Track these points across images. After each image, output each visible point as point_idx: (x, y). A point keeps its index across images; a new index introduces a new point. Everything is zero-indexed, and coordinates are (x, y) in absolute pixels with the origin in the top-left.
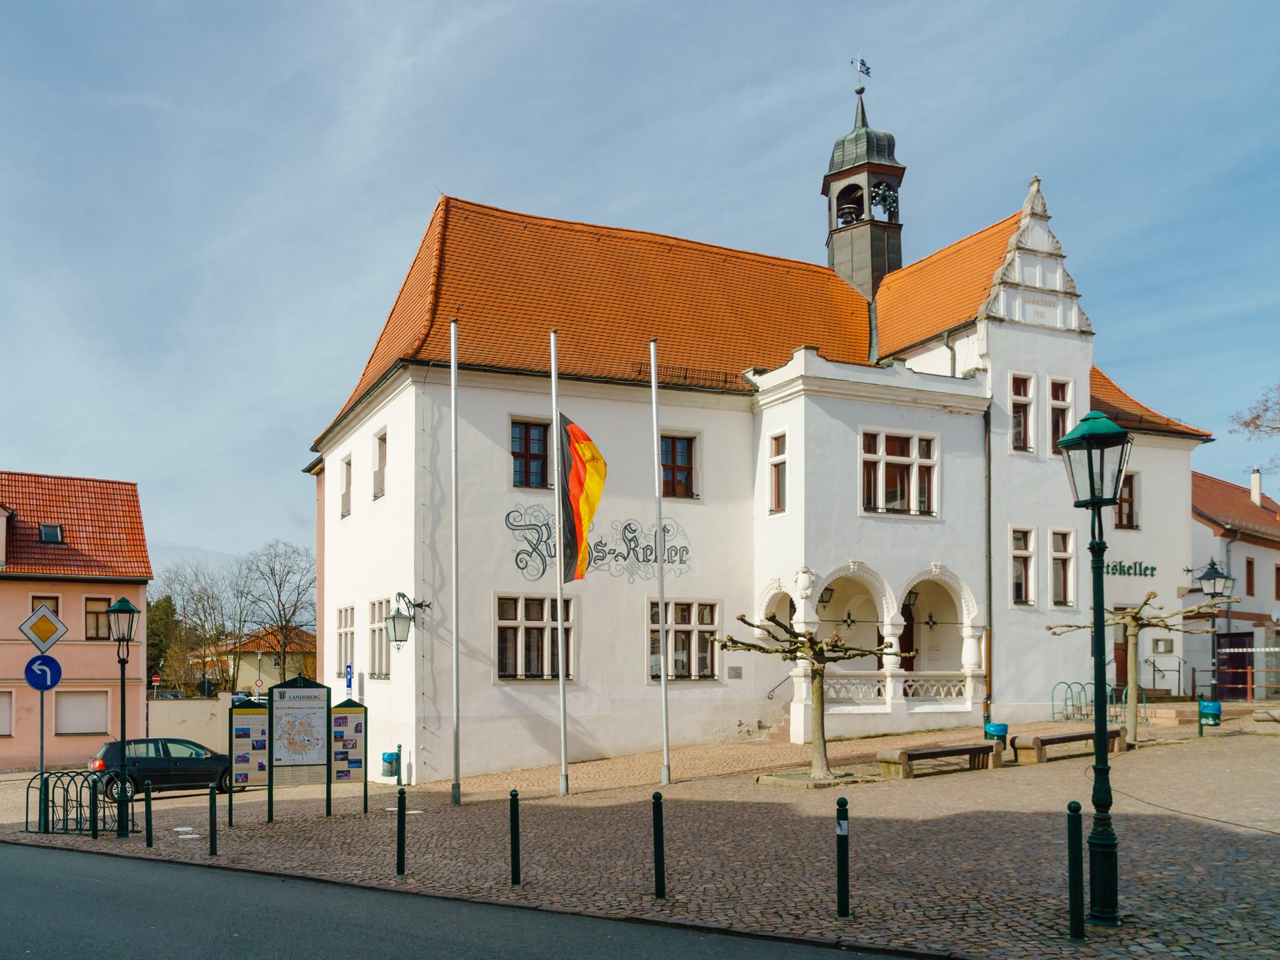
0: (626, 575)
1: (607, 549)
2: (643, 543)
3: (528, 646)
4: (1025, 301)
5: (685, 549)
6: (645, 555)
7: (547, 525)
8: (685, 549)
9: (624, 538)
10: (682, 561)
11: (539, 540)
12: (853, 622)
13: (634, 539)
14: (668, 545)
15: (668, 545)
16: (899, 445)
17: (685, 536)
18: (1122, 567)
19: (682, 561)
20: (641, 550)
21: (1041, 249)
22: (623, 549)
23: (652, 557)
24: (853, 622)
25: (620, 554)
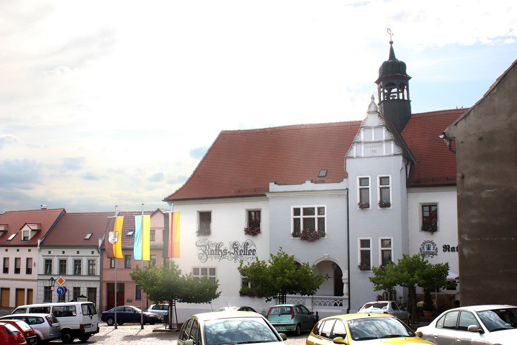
0: (234, 260)
1: (227, 252)
2: (240, 248)
3: (341, 305)
4: (365, 147)
5: (255, 250)
6: (240, 253)
7: (208, 245)
8: (255, 250)
9: (233, 248)
10: (253, 254)
11: (206, 250)
12: (329, 277)
13: (237, 248)
14: (248, 249)
15: (248, 249)
16: (308, 211)
17: (255, 245)
18: (218, 249)
19: (253, 254)
20: (218, 251)
21: (371, 126)
22: (233, 251)
23: (243, 253)
24: (329, 277)
25: (232, 253)
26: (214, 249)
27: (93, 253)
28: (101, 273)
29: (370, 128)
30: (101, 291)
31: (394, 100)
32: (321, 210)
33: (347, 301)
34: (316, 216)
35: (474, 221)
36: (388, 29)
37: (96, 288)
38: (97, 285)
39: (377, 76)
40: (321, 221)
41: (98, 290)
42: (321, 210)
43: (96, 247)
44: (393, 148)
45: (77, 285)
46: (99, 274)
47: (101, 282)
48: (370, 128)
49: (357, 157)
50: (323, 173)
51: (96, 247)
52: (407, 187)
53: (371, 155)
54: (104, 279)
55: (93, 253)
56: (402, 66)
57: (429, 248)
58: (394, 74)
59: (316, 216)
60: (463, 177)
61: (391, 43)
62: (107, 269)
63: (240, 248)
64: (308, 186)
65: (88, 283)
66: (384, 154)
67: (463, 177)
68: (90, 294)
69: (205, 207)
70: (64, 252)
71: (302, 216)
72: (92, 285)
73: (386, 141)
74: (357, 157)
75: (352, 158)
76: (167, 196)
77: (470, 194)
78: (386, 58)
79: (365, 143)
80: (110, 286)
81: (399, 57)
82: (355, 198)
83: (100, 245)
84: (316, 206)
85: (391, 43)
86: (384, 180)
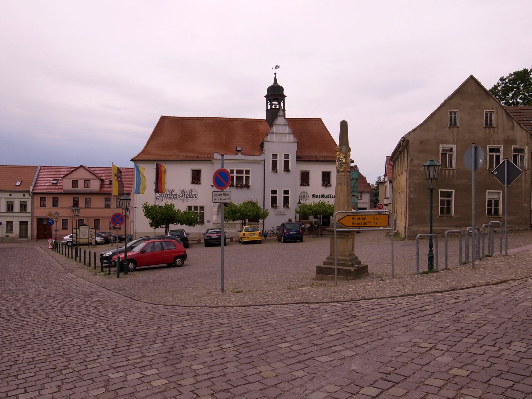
2: (186, 194)
17: (197, 192)
26: (168, 193)
27: (24, 195)
28: (32, 210)
29: (279, 125)
30: (32, 224)
31: (275, 109)
32: (248, 172)
33: (262, 225)
34: (244, 175)
35: (416, 181)
36: (279, 67)
37: (27, 222)
38: (29, 220)
39: (266, 93)
40: (247, 178)
41: (29, 223)
42: (248, 172)
43: (28, 191)
44: (292, 138)
45: (10, 219)
46: (30, 211)
47: (32, 217)
48: (279, 125)
49: (271, 142)
50: (239, 149)
51: (28, 191)
52: (297, 161)
53: (280, 141)
54: (34, 215)
55: (24, 195)
56: (281, 89)
57: (304, 196)
58: (275, 93)
59: (244, 175)
60: (412, 160)
61: (275, 74)
62: (37, 208)
63: (186, 194)
64: (240, 156)
65: (6, 218)
66: (287, 141)
67: (412, 160)
68: (22, 226)
69: (196, 167)
70: (10, 195)
71: (235, 175)
72: (24, 220)
73: (289, 134)
74: (271, 142)
75: (268, 142)
76: (132, 157)
77: (415, 168)
78: (271, 83)
79: (276, 133)
80: (40, 220)
81: (280, 83)
82: (269, 165)
83: (31, 190)
84: (244, 169)
85: (275, 74)
86: (287, 156)
